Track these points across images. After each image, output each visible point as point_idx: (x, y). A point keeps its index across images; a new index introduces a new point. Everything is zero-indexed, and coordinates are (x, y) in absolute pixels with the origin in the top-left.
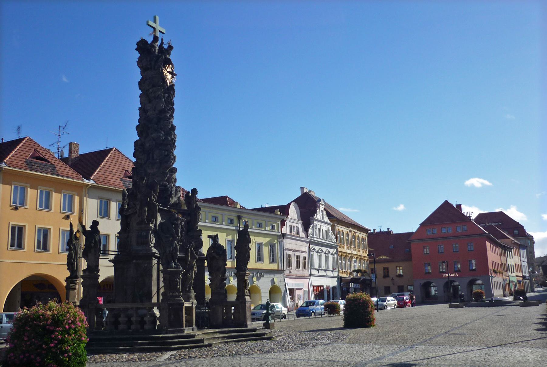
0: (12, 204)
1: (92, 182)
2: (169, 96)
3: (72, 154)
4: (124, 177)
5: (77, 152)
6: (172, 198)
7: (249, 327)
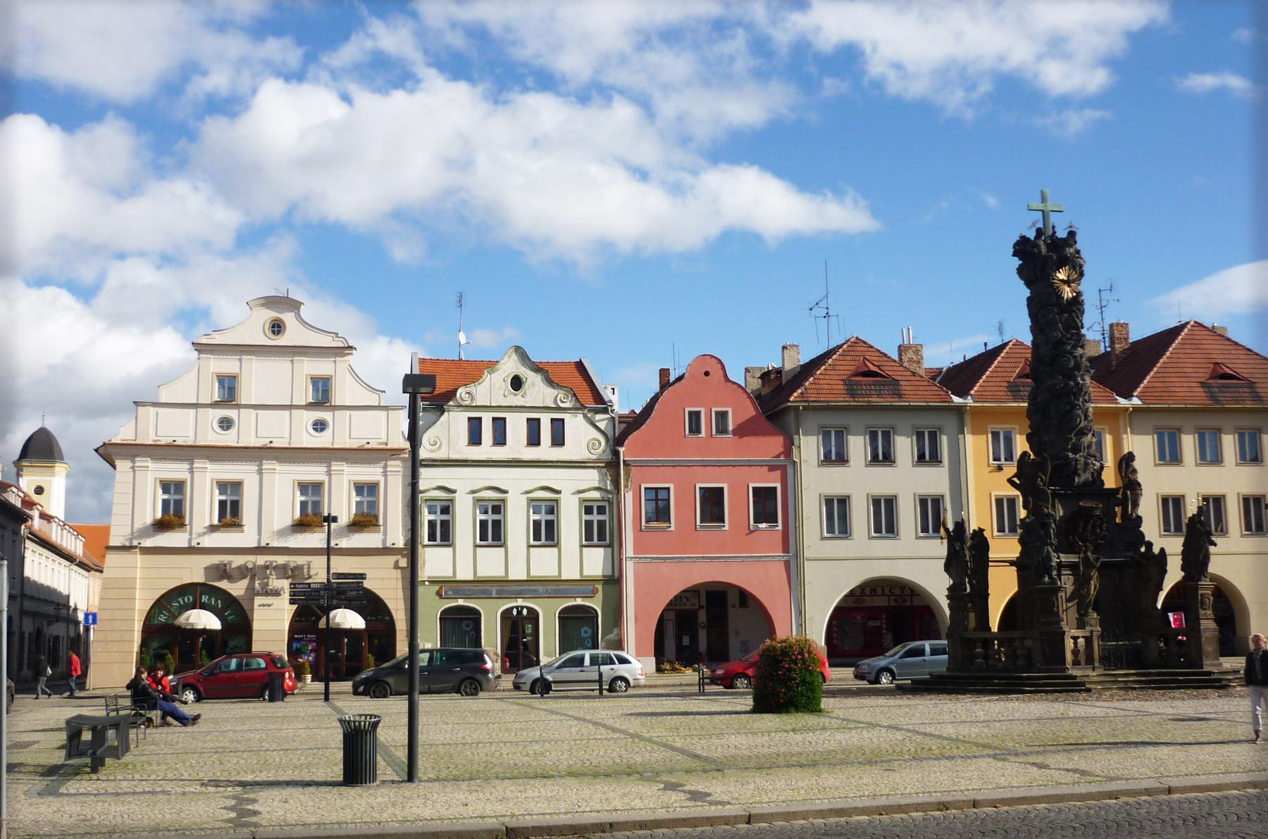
0: (991, 461)
1: (1136, 401)
2: (1071, 316)
3: (1117, 346)
4: (1211, 378)
5: (1126, 339)
6: (1079, 476)
7: (1206, 669)
